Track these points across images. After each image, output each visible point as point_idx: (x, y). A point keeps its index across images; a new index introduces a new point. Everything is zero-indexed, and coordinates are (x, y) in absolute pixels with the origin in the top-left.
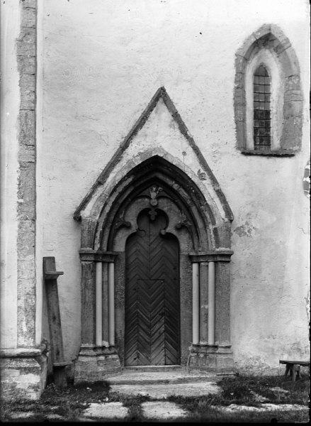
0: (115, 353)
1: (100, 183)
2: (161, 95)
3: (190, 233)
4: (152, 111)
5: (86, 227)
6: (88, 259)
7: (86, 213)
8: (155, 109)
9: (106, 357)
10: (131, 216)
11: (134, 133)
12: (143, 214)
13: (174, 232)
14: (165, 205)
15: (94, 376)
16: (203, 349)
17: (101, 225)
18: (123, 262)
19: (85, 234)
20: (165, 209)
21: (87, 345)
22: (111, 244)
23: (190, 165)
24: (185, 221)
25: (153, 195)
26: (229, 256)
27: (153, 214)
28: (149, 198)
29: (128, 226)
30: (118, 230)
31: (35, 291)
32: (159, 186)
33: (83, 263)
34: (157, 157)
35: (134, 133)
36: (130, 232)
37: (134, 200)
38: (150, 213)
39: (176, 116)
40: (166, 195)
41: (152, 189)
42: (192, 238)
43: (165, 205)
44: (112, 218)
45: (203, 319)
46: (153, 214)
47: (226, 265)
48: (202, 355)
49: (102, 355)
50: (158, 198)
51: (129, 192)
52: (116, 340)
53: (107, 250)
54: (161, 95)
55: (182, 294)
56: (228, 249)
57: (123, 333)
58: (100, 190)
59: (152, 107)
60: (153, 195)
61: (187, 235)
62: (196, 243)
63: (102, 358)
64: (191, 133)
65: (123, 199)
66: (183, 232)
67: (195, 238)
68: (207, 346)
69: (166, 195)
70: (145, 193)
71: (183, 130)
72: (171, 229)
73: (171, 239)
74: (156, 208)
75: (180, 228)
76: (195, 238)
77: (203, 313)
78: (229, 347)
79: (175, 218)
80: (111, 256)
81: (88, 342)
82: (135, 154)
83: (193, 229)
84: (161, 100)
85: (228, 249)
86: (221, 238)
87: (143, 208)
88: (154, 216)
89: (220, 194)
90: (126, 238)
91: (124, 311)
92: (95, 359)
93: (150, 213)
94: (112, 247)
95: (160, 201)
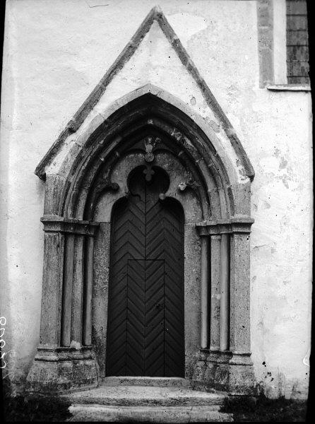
0: (90, 358)
1: (71, 130)
2: (156, 19)
3: (199, 198)
4: (142, 37)
5: (51, 187)
6: (53, 229)
7: (51, 171)
8: (147, 35)
9: (75, 364)
10: (120, 177)
11: (119, 65)
12: (135, 177)
13: (178, 197)
14: (164, 161)
15: (51, 390)
16: (212, 357)
17: (74, 185)
18: (107, 236)
19: (50, 198)
20: (166, 166)
21: (47, 346)
22: (90, 212)
23: (199, 112)
24: (191, 182)
25: (149, 148)
26: (249, 225)
27: (149, 173)
28: (144, 152)
29: (114, 189)
30: (101, 194)
31: (93, 281)
32: (155, 138)
33: (47, 234)
34: (149, 94)
35: (119, 65)
36: (119, 196)
37: (124, 155)
38: (145, 172)
39: (176, 44)
40: (168, 149)
41: (147, 141)
42: (200, 204)
43: (164, 161)
44: (91, 177)
45: (213, 313)
46: (149, 173)
47: (244, 238)
48: (211, 366)
49: (69, 360)
50: (155, 152)
51: (114, 144)
52: (94, 340)
53: (84, 219)
54: (156, 19)
55: (186, 278)
56: (246, 216)
57: (105, 330)
58: (72, 141)
59: (140, 35)
60: (149, 148)
61: (195, 200)
62: (206, 210)
63: (68, 364)
64: (196, 60)
65: (107, 153)
66: (188, 196)
67: (205, 204)
68: (218, 353)
69: (168, 149)
70: (138, 146)
71: (183, 57)
72: (171, 192)
73: (174, 208)
74: (152, 165)
75: (188, 190)
76: (205, 204)
77: (213, 306)
78: (249, 355)
79: (178, 183)
80: (89, 227)
81: (49, 341)
82: (119, 93)
83: (202, 191)
84: (156, 23)
85: (246, 216)
86: (237, 201)
87: (135, 165)
88: (148, 180)
89: (234, 140)
90: (113, 203)
91: (106, 302)
92: (55, 366)
93: (145, 172)
94: (93, 217)
95: (159, 156)
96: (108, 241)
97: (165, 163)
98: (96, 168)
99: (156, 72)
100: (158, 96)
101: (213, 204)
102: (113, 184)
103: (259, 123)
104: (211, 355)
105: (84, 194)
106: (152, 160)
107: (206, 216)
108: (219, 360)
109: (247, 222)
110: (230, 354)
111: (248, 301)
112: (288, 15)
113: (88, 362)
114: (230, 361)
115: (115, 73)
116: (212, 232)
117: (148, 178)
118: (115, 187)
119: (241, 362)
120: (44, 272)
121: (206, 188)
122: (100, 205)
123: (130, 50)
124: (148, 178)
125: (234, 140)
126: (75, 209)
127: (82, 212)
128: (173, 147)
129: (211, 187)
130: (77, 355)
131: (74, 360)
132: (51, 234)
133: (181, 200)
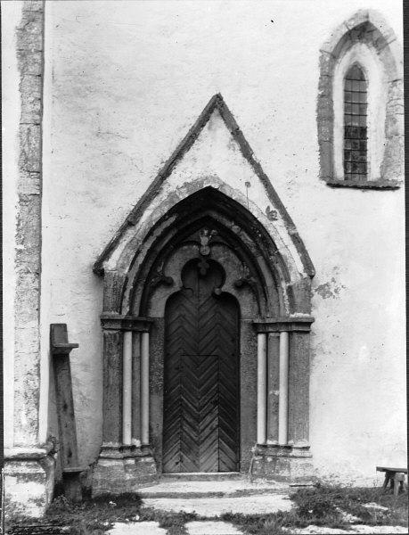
2: (217, 106)
4: (203, 126)
7: (111, 265)
9: (137, 461)
10: (173, 270)
12: (189, 268)
13: (233, 292)
14: (222, 256)
16: (271, 451)
20: (221, 260)
21: (110, 444)
22: (145, 306)
23: (257, 202)
25: (204, 240)
26: (309, 324)
27: (203, 266)
28: (199, 245)
29: (168, 283)
30: (155, 288)
33: (106, 332)
34: (210, 188)
38: (199, 265)
39: (237, 134)
41: (203, 233)
42: (257, 300)
43: (222, 256)
44: (147, 271)
46: (203, 266)
47: (305, 337)
50: (210, 245)
51: (170, 236)
53: (140, 316)
56: (307, 315)
58: (131, 233)
60: (204, 240)
61: (251, 296)
62: (263, 307)
63: (131, 462)
65: (163, 245)
66: (245, 292)
70: (193, 237)
71: (247, 152)
72: (228, 287)
73: (229, 302)
74: (208, 259)
78: (307, 448)
83: (259, 287)
85: (307, 315)
86: (298, 300)
87: (190, 257)
89: (296, 239)
91: (162, 398)
92: (121, 463)
93: (199, 265)
95: (214, 249)
96: (162, 336)
97: (220, 256)
98: (151, 261)
99: (215, 164)
100: (220, 190)
101: (272, 300)
102: (168, 278)
103: (335, 235)
104: (270, 449)
105: (140, 288)
106: (207, 253)
107: (262, 311)
108: (279, 454)
109: (307, 321)
110: (289, 448)
111: (308, 397)
112: (345, 91)
113: (148, 460)
114: (291, 454)
115: (175, 164)
116: (270, 330)
117: (203, 272)
118: (169, 282)
119: (300, 455)
120: (104, 370)
121: (263, 284)
122: (153, 299)
123: (192, 137)
124: (203, 272)
125: (296, 239)
126: (131, 305)
127: (138, 309)
128: (232, 242)
129: (269, 282)
130: (138, 452)
131: (136, 458)
132: (111, 332)
133: (237, 296)
